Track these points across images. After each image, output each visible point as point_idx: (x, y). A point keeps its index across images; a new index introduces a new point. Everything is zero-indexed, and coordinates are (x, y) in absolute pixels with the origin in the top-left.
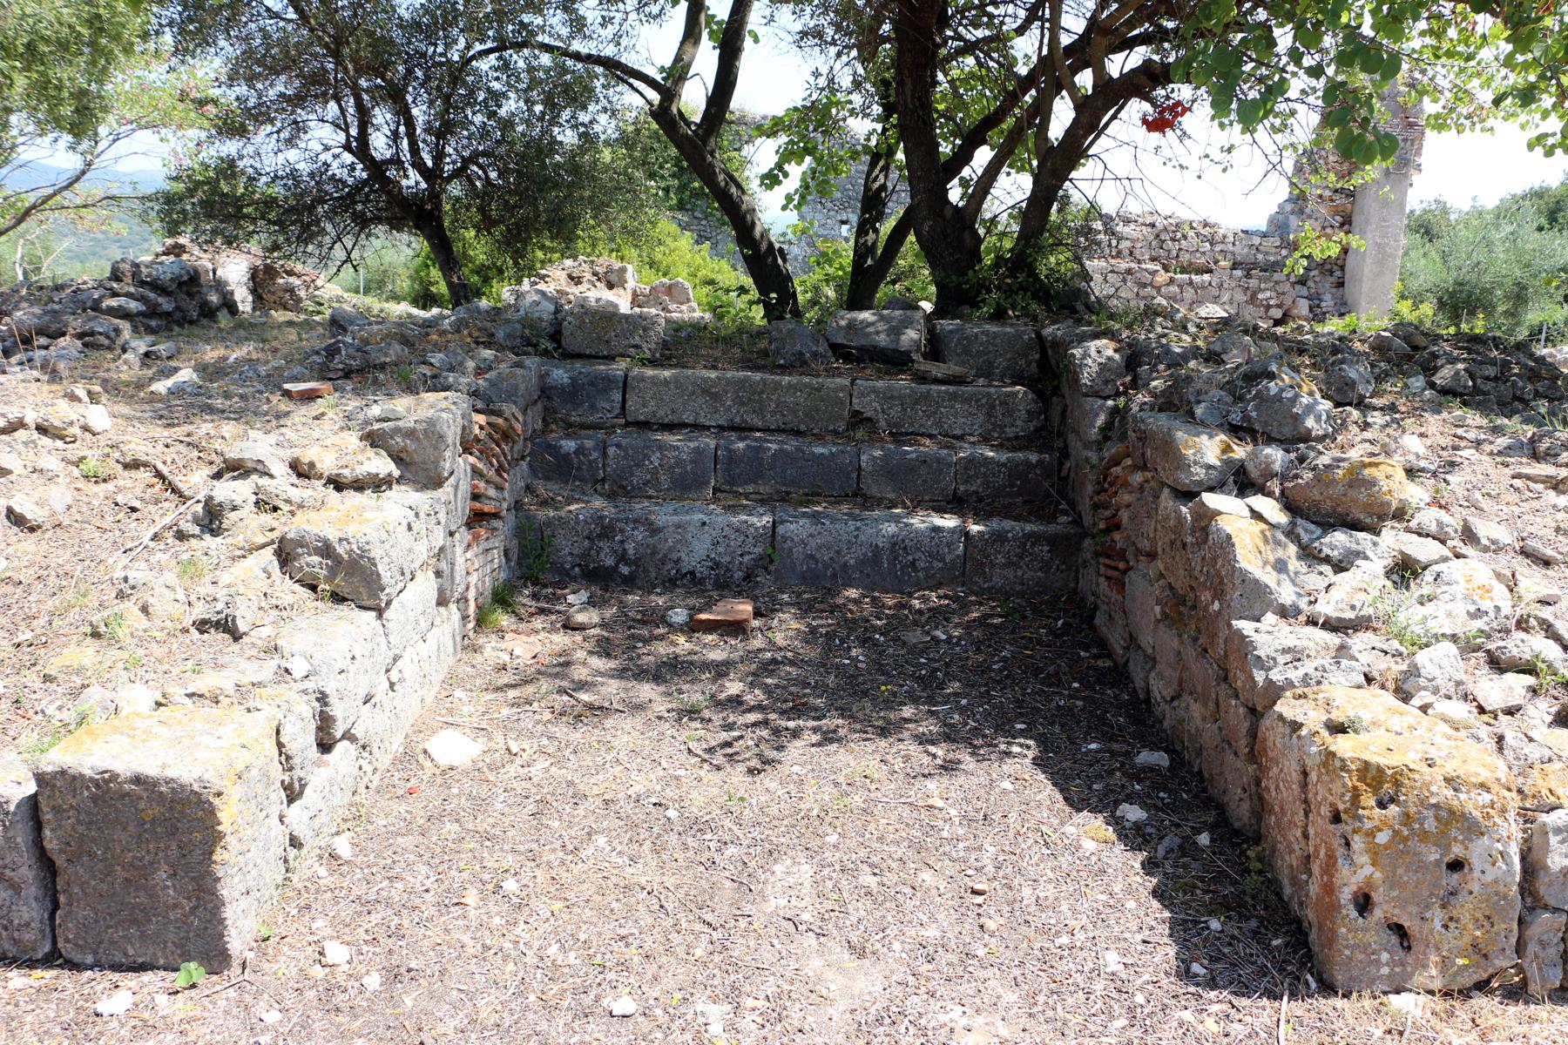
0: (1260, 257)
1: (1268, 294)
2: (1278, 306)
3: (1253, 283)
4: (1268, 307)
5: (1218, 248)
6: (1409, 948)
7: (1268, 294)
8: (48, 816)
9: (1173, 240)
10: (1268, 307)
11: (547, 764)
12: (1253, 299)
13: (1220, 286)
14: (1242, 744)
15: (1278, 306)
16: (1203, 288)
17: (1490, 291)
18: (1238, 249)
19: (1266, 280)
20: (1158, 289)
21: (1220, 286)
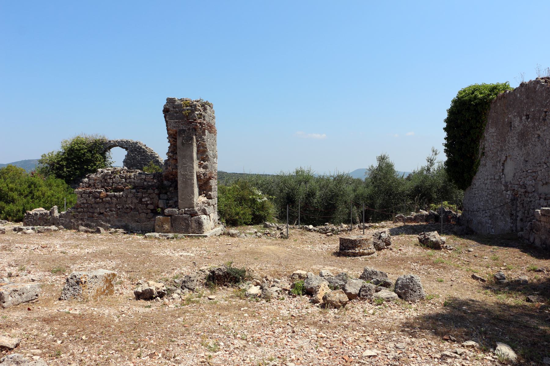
0: (145, 183)
1: (147, 199)
2: (151, 204)
3: (140, 195)
4: (147, 205)
5: (128, 181)
6: (318, 286)
7: (147, 199)
8: (55, 310)
9: (110, 178)
10: (147, 205)
11: (189, 284)
12: (141, 202)
13: (127, 197)
14: (502, 162)
15: (151, 204)
16: (120, 198)
17: (276, 201)
18: (136, 181)
19: (145, 193)
20: (102, 199)
21: (127, 197)
